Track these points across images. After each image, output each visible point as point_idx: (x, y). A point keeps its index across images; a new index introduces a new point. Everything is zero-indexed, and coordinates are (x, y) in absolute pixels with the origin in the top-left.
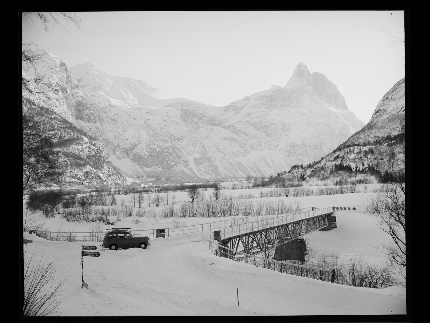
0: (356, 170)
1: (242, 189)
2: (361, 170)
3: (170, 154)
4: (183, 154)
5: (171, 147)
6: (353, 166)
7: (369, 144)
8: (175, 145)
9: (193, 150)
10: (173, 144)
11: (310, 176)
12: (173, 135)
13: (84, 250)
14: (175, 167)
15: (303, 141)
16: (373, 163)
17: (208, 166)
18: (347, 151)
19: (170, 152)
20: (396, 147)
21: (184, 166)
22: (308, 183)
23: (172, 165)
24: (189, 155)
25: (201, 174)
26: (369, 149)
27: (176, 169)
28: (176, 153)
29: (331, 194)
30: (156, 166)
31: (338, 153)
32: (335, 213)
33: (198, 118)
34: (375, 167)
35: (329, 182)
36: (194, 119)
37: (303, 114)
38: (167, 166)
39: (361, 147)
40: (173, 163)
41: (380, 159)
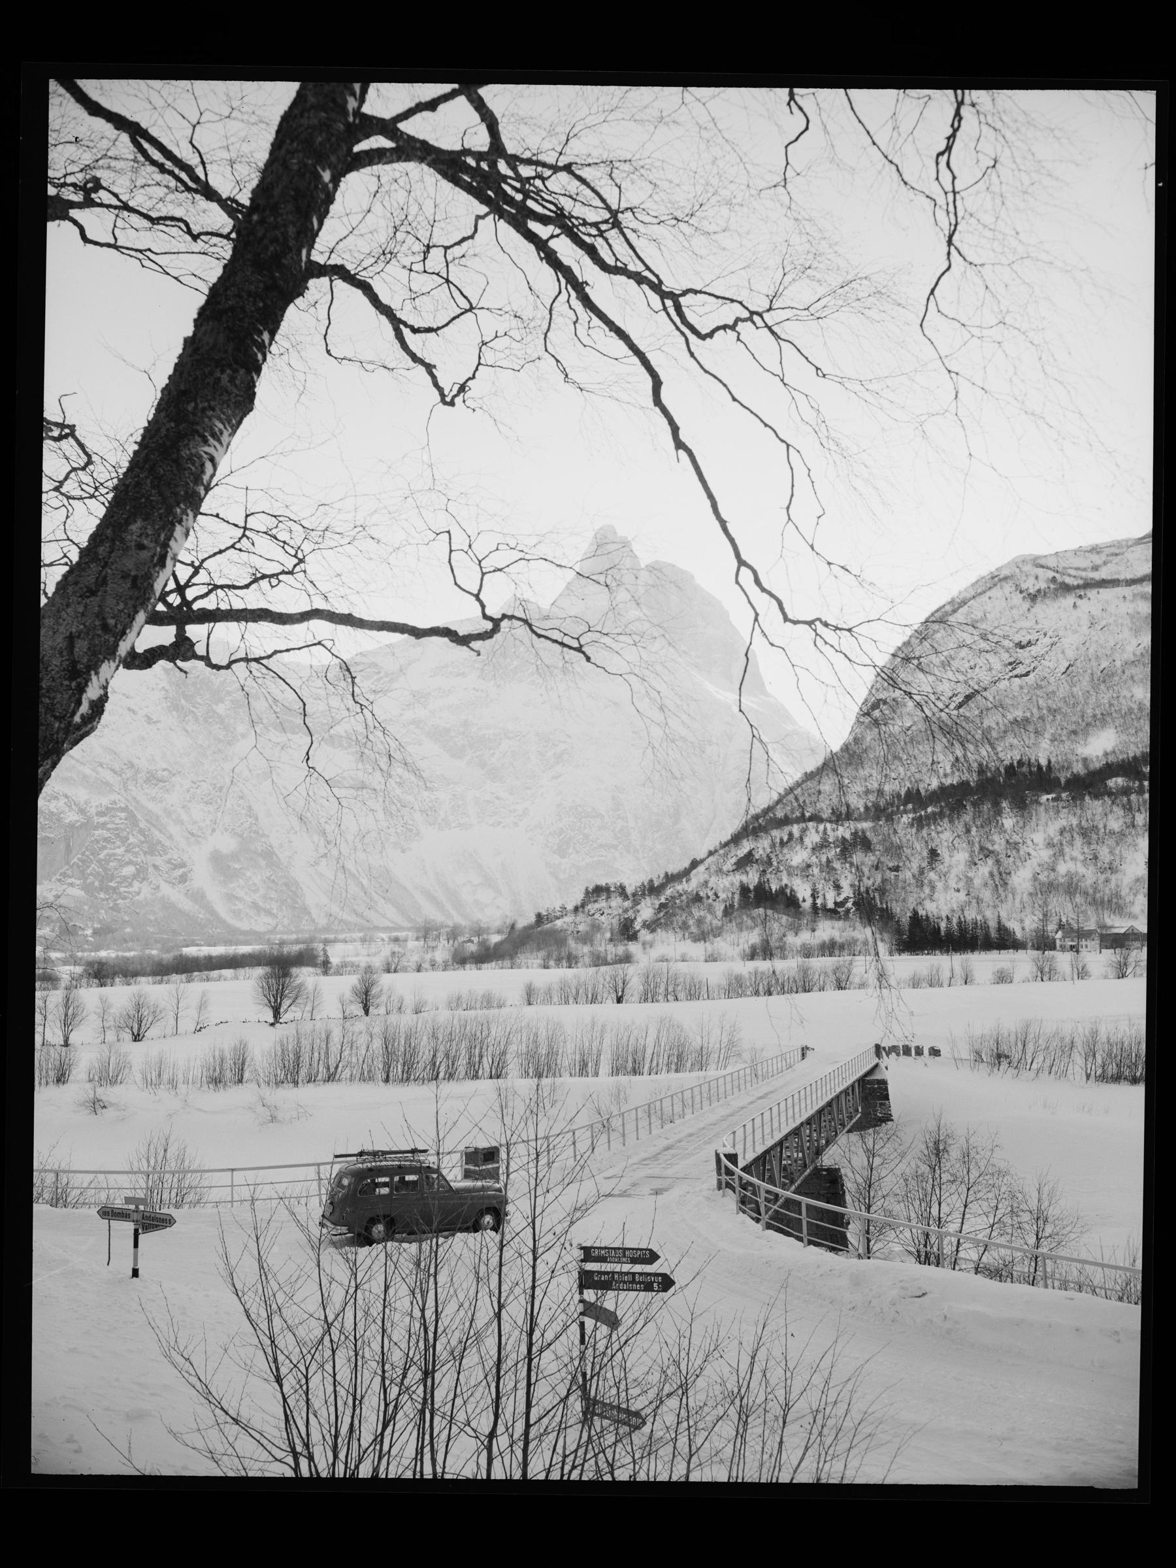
0: (814, 905)
1: (419, 971)
2: (830, 905)
3: (118, 836)
4: (171, 837)
5: (123, 810)
6: (803, 891)
7: (849, 816)
8: (138, 802)
9: (208, 822)
10: (129, 798)
11: (651, 926)
12: (131, 765)
13: (591, 1266)
14: (136, 885)
15: (613, 798)
16: (870, 883)
17: (264, 882)
18: (781, 840)
19: (117, 829)
20: (939, 829)
21: (170, 883)
22: (648, 949)
23: (125, 878)
24: (193, 839)
25: (237, 914)
26: (855, 834)
27: (138, 894)
28: (141, 832)
29: (770, 994)
30: (59, 880)
31: (746, 846)
32: (882, 1066)
33: (232, 701)
34: (876, 895)
35: (721, 945)
36: (214, 707)
37: (615, 704)
38: (101, 881)
39: (828, 825)
40: (129, 870)
41: (890, 869)
